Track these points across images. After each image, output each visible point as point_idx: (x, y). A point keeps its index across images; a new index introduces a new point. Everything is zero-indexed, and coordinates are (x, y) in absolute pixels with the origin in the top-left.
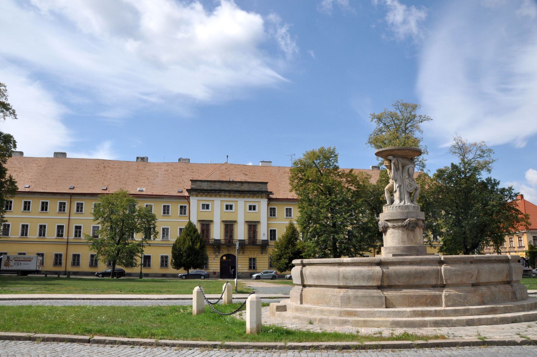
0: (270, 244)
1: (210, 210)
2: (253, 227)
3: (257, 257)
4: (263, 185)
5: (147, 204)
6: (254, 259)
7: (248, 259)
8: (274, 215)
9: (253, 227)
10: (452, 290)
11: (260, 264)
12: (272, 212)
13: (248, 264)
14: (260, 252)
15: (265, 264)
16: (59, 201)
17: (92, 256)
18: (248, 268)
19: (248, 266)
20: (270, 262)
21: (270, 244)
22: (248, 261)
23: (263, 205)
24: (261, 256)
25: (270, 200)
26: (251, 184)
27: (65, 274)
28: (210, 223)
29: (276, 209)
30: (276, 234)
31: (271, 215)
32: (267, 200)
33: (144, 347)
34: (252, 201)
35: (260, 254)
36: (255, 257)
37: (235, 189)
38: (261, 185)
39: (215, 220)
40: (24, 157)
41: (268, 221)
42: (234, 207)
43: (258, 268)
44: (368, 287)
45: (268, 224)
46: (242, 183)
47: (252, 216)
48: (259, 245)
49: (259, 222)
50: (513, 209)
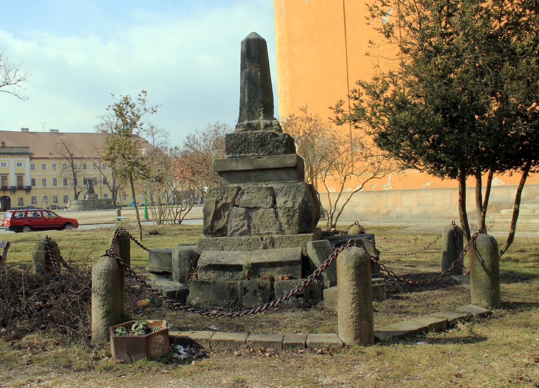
0: (32, 188)
1: (7, 166)
2: (20, 177)
4: (27, 149)
6: (22, 199)
8: (34, 169)
9: (20, 177)
12: (33, 167)
17: (35, 185)
18: (31, 203)
23: (26, 161)
25: (31, 159)
26: (18, 148)
31: (32, 169)
33: (496, 29)
34: (19, 159)
37: (8, 152)
38: (24, 149)
41: (30, 173)
42: (22, 164)
45: (30, 175)
46: (12, 147)
47: (20, 170)
48: (24, 189)
50: (188, 358)
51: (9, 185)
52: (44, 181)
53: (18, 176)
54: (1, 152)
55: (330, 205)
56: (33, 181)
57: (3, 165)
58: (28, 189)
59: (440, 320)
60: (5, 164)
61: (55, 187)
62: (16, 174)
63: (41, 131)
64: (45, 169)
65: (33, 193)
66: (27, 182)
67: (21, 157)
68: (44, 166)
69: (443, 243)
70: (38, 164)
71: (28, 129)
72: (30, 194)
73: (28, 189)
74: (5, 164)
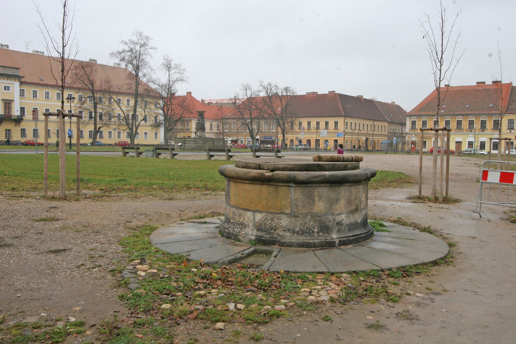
1: (11, 91)
3: (12, 128)
4: (16, 70)
5: (34, 90)
6: (9, 130)
7: (5, 130)
11: (14, 134)
12: (22, 93)
13: (5, 134)
14: (14, 125)
16: (45, 91)
18: (5, 137)
19: (5, 136)
20: (243, 148)
21: (24, 119)
22: (5, 132)
23: (16, 86)
24: (15, 128)
25: (22, 83)
27: (200, 149)
28: (11, 102)
29: (38, 92)
30: (24, 110)
31: (20, 95)
32: (19, 83)
35: (14, 126)
36: (10, 129)
38: (13, 69)
39: (15, 100)
41: (20, 100)
42: (11, 88)
43: (13, 138)
44: (285, 169)
45: (20, 102)
49: (13, 101)
51: (13, 114)
52: (35, 111)
53: (5, 103)
54: (2, 72)
55: (421, 168)
56: (22, 110)
57: (6, 88)
58: (18, 121)
60: (9, 87)
61: (211, 131)
62: (3, 100)
63: (25, 51)
64: (36, 97)
65: (23, 125)
66: (16, 112)
67: (9, 79)
68: (35, 94)
69: (436, 91)
70: (29, 91)
71: (8, 47)
72: (19, 126)
73: (18, 121)
74: (9, 87)
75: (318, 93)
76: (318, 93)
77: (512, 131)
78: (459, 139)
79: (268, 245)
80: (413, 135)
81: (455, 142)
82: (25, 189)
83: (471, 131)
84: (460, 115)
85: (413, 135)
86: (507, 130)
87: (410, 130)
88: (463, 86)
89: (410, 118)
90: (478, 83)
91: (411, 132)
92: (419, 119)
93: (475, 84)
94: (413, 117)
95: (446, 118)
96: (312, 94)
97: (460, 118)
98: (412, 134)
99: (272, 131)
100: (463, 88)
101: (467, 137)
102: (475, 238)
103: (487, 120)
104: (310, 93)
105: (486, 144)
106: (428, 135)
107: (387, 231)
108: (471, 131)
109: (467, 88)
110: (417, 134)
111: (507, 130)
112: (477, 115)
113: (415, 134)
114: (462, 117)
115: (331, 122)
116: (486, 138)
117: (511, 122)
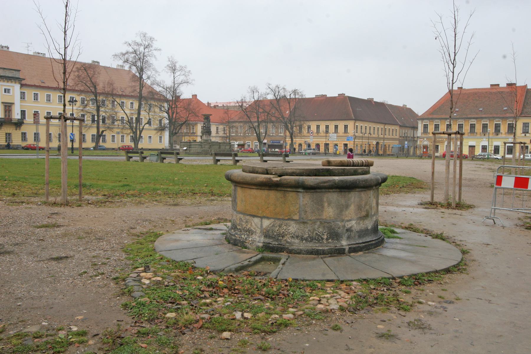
1: (11, 94)
3: (13, 132)
4: (17, 72)
5: (35, 92)
6: (10, 134)
7: (5, 134)
10: (275, 144)
11: (15, 138)
12: (23, 96)
13: (5, 138)
14: (15, 128)
15: (19, 136)
16: (46, 94)
18: (5, 141)
19: (5, 140)
21: (25, 122)
22: (5, 136)
23: (16, 88)
24: (16, 132)
25: (22, 86)
28: (12, 105)
29: (39, 95)
30: (25, 113)
31: (21, 98)
32: (20, 85)
35: (15, 130)
36: (10, 132)
38: (14, 72)
39: (15, 103)
40: (504, 188)
41: (21, 103)
42: (11, 91)
43: (13, 142)
45: (21, 105)
49: (13, 103)
51: (13, 117)
52: (36, 114)
53: (5, 106)
54: (2, 75)
55: (433, 173)
56: (23, 113)
57: (7, 91)
58: (19, 124)
59: (280, 253)
60: (9, 90)
61: (217, 135)
62: (3, 103)
63: (25, 52)
64: (37, 99)
65: (24, 129)
66: (16, 115)
67: (10, 82)
68: (36, 96)
70: (30, 93)
71: (8, 48)
72: (20, 129)
73: (19, 124)
74: (9, 90)
75: (327, 96)
76: (327, 96)
77: (527, 135)
78: (472, 143)
79: (276, 253)
80: (425, 139)
81: (468, 146)
82: (26, 195)
83: (485, 135)
84: (474, 118)
85: (425, 139)
86: (521, 133)
87: (422, 134)
88: (476, 89)
89: (422, 121)
90: (491, 85)
91: (423, 136)
92: (431, 123)
93: (489, 87)
94: (425, 121)
95: (459, 122)
96: (321, 97)
97: (473, 122)
98: (423, 138)
99: (279, 135)
100: (476, 91)
101: (481, 141)
102: (489, 245)
103: (501, 123)
104: (319, 96)
105: (500, 148)
106: (441, 139)
107: (398, 238)
108: (485, 135)
109: (480, 91)
110: (429, 138)
111: (521, 133)
112: (491, 119)
113: (427, 138)
114: (476, 121)
115: (341, 125)
116: (500, 142)
117: (526, 125)
